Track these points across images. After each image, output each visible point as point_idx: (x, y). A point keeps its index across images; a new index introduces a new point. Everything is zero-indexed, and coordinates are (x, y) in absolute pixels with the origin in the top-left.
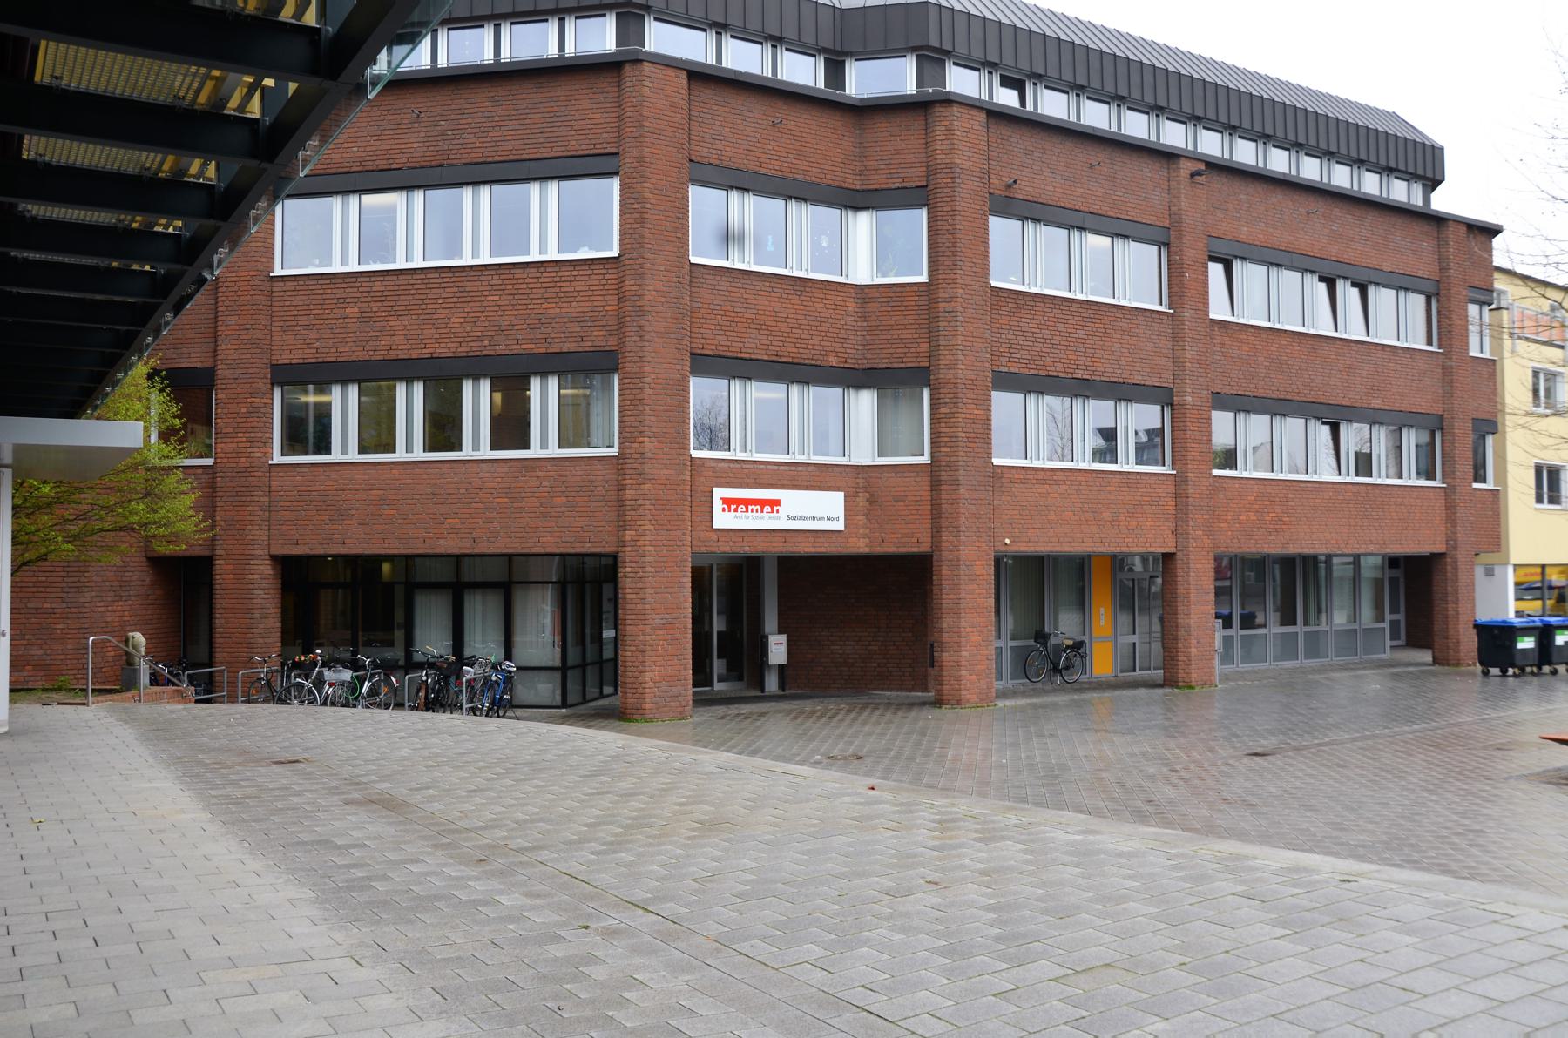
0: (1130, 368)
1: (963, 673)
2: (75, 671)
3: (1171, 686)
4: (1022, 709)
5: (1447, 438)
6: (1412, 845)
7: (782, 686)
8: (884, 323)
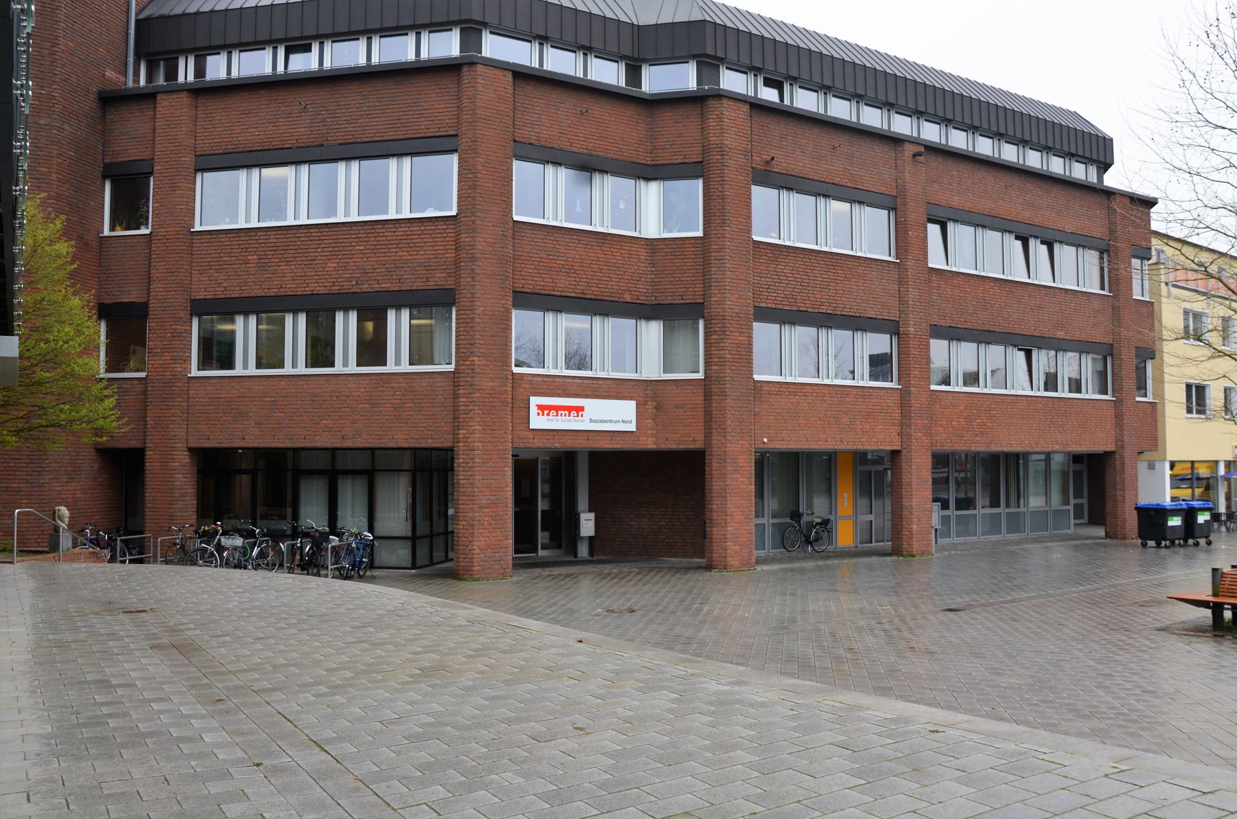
0: (865, 305)
1: (729, 544)
2: (36, 537)
3: (898, 555)
4: (776, 572)
5: (1117, 362)
6: (1051, 687)
7: (591, 553)
8: (669, 268)
